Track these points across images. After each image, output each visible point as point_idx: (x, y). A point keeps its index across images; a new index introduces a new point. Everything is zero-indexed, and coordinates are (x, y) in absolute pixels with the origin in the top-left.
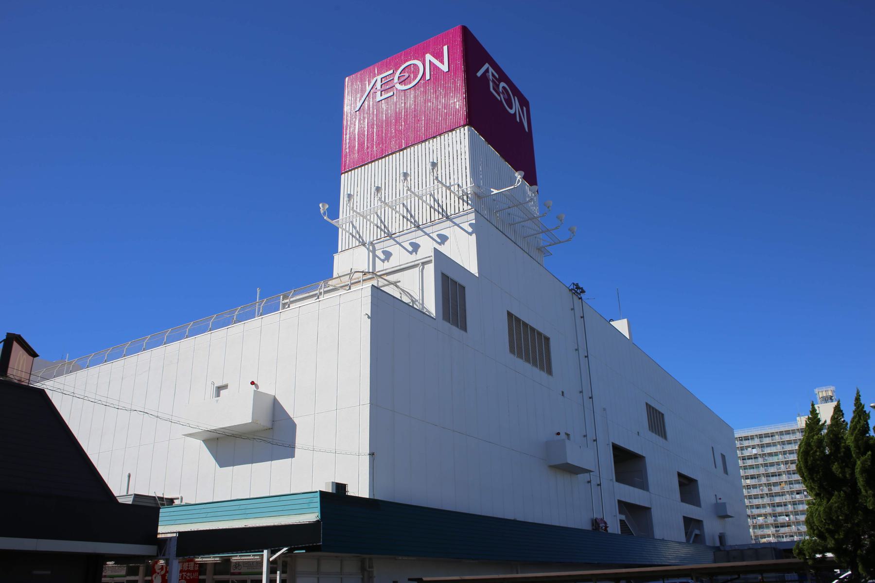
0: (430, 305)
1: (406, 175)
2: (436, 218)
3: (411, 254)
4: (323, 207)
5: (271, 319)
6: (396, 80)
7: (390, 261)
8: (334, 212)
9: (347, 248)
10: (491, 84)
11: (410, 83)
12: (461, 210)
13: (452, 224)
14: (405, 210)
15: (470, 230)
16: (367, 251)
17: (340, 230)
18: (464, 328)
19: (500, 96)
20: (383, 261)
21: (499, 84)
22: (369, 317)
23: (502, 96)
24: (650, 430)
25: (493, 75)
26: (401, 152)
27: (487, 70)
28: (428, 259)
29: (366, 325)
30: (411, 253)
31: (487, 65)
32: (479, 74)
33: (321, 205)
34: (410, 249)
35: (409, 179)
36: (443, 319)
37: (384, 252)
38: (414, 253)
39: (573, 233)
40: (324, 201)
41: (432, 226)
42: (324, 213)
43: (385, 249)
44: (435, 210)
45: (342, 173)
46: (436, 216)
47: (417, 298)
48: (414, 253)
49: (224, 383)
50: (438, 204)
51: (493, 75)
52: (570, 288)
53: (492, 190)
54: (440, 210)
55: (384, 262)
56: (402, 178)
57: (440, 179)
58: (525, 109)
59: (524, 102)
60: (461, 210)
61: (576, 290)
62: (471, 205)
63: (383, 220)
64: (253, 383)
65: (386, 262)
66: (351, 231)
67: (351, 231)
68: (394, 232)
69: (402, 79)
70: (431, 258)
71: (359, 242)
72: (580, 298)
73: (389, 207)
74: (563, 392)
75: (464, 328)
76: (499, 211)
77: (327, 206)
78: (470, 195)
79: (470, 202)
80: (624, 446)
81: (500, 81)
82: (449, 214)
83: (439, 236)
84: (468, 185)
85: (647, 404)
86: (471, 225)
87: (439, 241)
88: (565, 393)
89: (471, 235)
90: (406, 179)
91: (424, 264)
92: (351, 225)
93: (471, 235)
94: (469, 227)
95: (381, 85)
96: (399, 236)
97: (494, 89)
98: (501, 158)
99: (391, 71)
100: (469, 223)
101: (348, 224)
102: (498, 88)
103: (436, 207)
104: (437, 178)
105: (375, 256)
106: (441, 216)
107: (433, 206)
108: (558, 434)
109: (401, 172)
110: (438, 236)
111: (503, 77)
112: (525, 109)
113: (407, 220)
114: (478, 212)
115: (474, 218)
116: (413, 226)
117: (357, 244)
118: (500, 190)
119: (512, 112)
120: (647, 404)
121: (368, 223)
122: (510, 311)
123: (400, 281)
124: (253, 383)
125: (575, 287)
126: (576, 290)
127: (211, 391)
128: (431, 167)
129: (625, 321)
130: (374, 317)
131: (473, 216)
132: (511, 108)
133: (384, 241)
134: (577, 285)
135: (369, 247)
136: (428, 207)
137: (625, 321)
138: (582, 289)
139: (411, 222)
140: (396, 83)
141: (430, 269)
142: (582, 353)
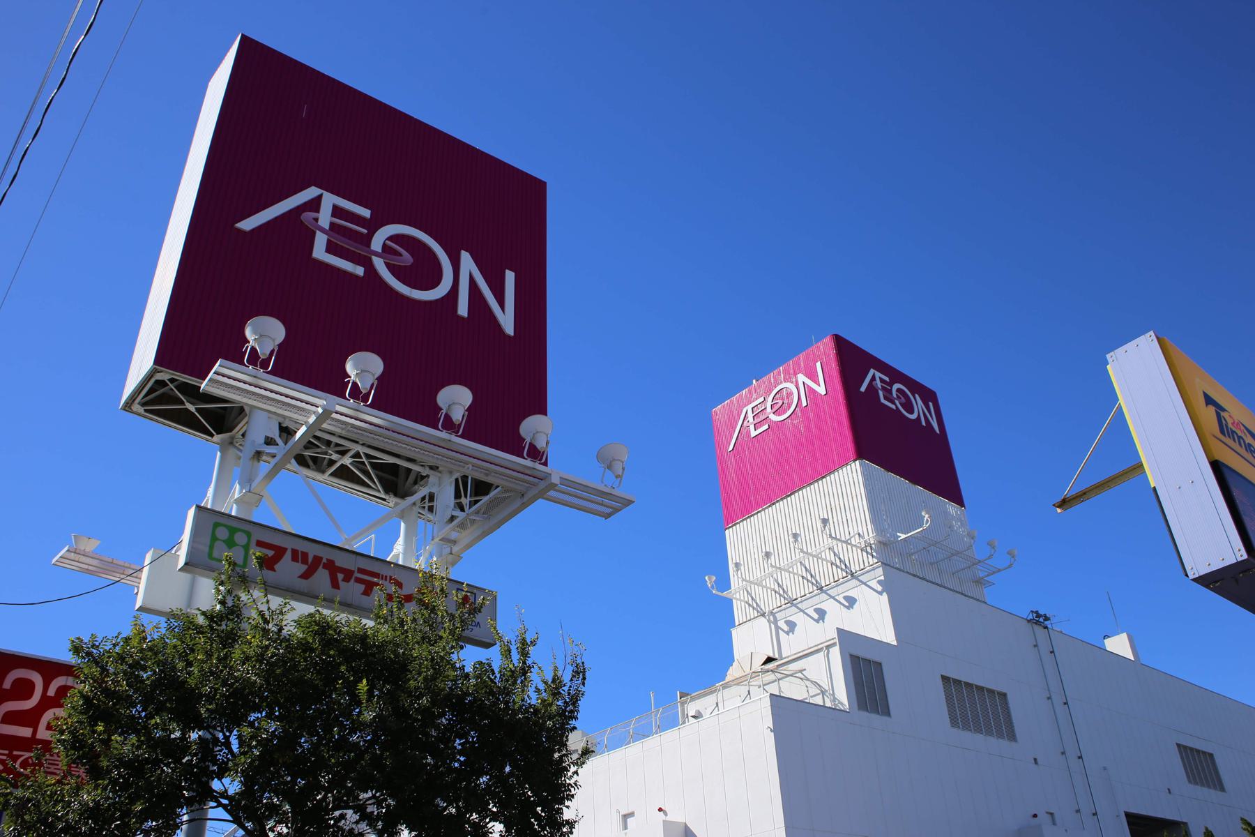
0: (842, 695)
1: (795, 536)
2: (840, 577)
3: (818, 623)
4: (710, 580)
5: (669, 737)
6: (769, 409)
7: (796, 632)
8: (724, 583)
9: (745, 620)
10: (881, 393)
11: (785, 412)
12: (867, 564)
13: (859, 583)
14: (804, 569)
15: (879, 588)
16: (768, 624)
17: (734, 601)
18: (887, 713)
19: (893, 403)
20: (787, 633)
21: (892, 388)
22: (771, 730)
23: (897, 402)
24: (1190, 782)
25: (882, 380)
26: (789, 498)
27: (873, 378)
28: (832, 642)
29: (770, 739)
30: (817, 621)
31: (872, 371)
32: (863, 389)
33: (706, 578)
34: (816, 616)
35: (799, 539)
36: (859, 709)
37: (788, 623)
38: (821, 621)
39: (1013, 557)
40: (710, 574)
41: (837, 586)
42: (712, 587)
43: (787, 619)
44: (837, 566)
45: (727, 529)
46: (841, 574)
47: (827, 688)
48: (821, 621)
49: (630, 811)
50: (840, 559)
51: (882, 380)
52: (1028, 619)
53: (898, 534)
54: (843, 567)
55: (788, 635)
56: (792, 540)
57: (833, 535)
58: (931, 404)
59: (929, 396)
60: (867, 564)
61: (1037, 619)
62: (876, 558)
63: (781, 583)
64: (660, 810)
65: (791, 634)
66: (746, 599)
67: (746, 599)
68: (794, 597)
69: (776, 407)
70: (835, 641)
71: (758, 612)
72: (1046, 627)
73: (785, 571)
74: (1035, 760)
75: (887, 713)
76: (918, 552)
77: (714, 578)
78: (873, 546)
79: (874, 554)
80: (1145, 814)
81: (891, 384)
82: (854, 571)
83: (846, 598)
84: (870, 535)
85: (1178, 745)
86: (880, 582)
87: (847, 604)
88: (1038, 760)
89: (881, 595)
90: (796, 541)
91: (828, 647)
92: (745, 592)
93: (881, 595)
94: (878, 586)
95: (754, 417)
96: (801, 602)
97: (885, 398)
98: (910, 484)
99: (762, 399)
100: (878, 579)
101: (741, 592)
102: (891, 393)
103: (838, 563)
104: (830, 536)
105: (777, 628)
106: (845, 574)
107: (834, 561)
108: (1035, 816)
109: (790, 533)
110: (845, 598)
111: (895, 375)
112: (931, 404)
113: (808, 581)
114: (886, 564)
115: (882, 573)
116: (815, 588)
117: (756, 615)
118: (908, 533)
119: (913, 417)
120: (1178, 745)
121: (765, 589)
122: (944, 674)
123: (805, 670)
124: (660, 810)
125: (1035, 615)
126: (1037, 619)
127: (618, 821)
128: (822, 525)
129: (1124, 636)
130: (779, 729)
131: (880, 571)
132: (912, 412)
133: (784, 609)
134: (1037, 612)
135: (769, 618)
136: (829, 564)
137: (1124, 636)
138: (1045, 615)
139: (813, 584)
140: (770, 413)
141: (836, 652)
142: (1058, 700)
